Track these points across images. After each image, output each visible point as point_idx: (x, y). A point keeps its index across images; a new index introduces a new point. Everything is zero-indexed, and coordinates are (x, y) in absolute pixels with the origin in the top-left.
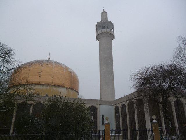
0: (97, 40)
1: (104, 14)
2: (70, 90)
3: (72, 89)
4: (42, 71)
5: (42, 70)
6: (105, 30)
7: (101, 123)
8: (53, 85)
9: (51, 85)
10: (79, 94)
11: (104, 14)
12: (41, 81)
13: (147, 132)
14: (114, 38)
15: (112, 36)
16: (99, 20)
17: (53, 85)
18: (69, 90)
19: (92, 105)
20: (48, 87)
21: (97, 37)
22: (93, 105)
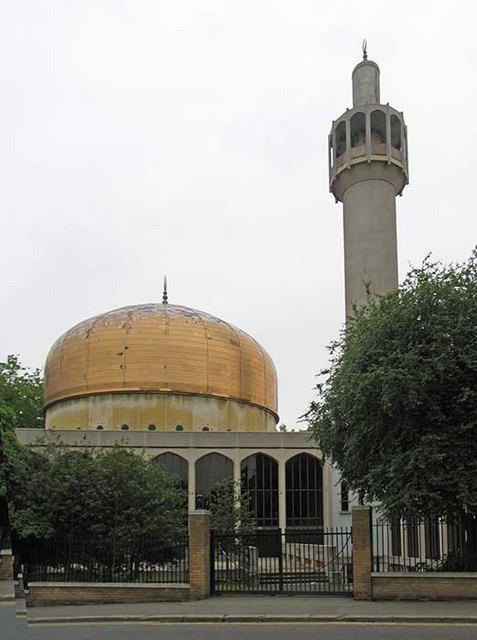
0: (338, 200)
1: (366, 74)
2: (235, 405)
3: (244, 402)
4: (126, 348)
5: (128, 343)
6: (368, 148)
7: (338, 506)
8: (169, 394)
9: (162, 393)
10: (277, 419)
11: (366, 74)
12: (126, 381)
13: (469, 571)
14: (405, 181)
15: (400, 177)
16: (341, 101)
17: (169, 394)
18: (230, 409)
19: (165, 450)
20: (154, 402)
21: (333, 189)
22: (170, 450)
